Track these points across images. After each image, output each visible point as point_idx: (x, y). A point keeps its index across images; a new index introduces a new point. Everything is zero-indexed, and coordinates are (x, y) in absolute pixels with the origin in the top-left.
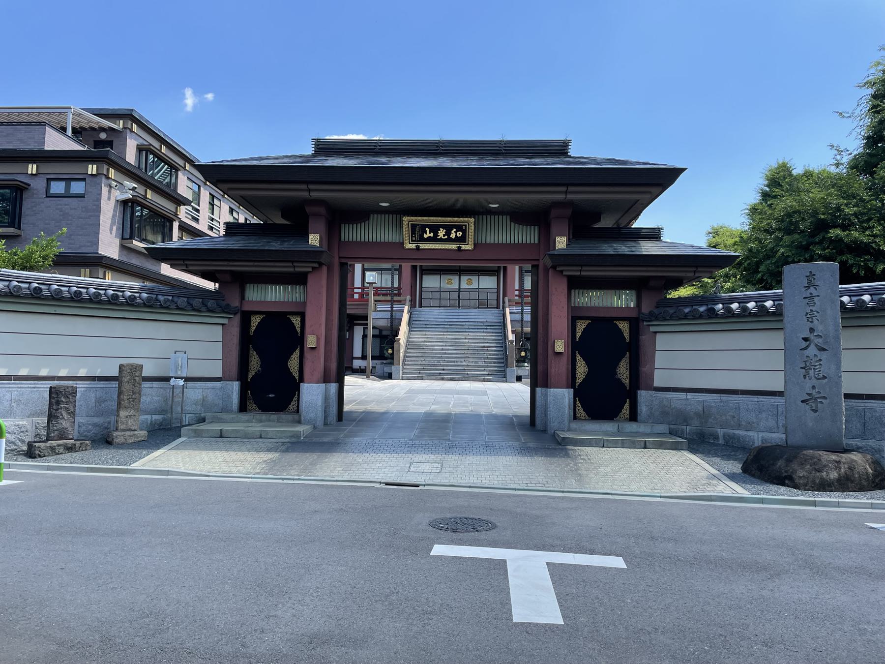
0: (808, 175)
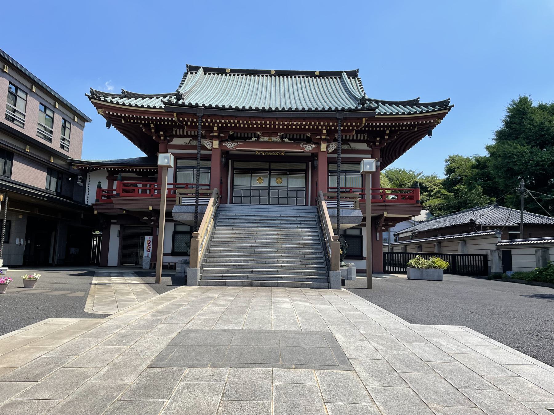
0: (542, 107)
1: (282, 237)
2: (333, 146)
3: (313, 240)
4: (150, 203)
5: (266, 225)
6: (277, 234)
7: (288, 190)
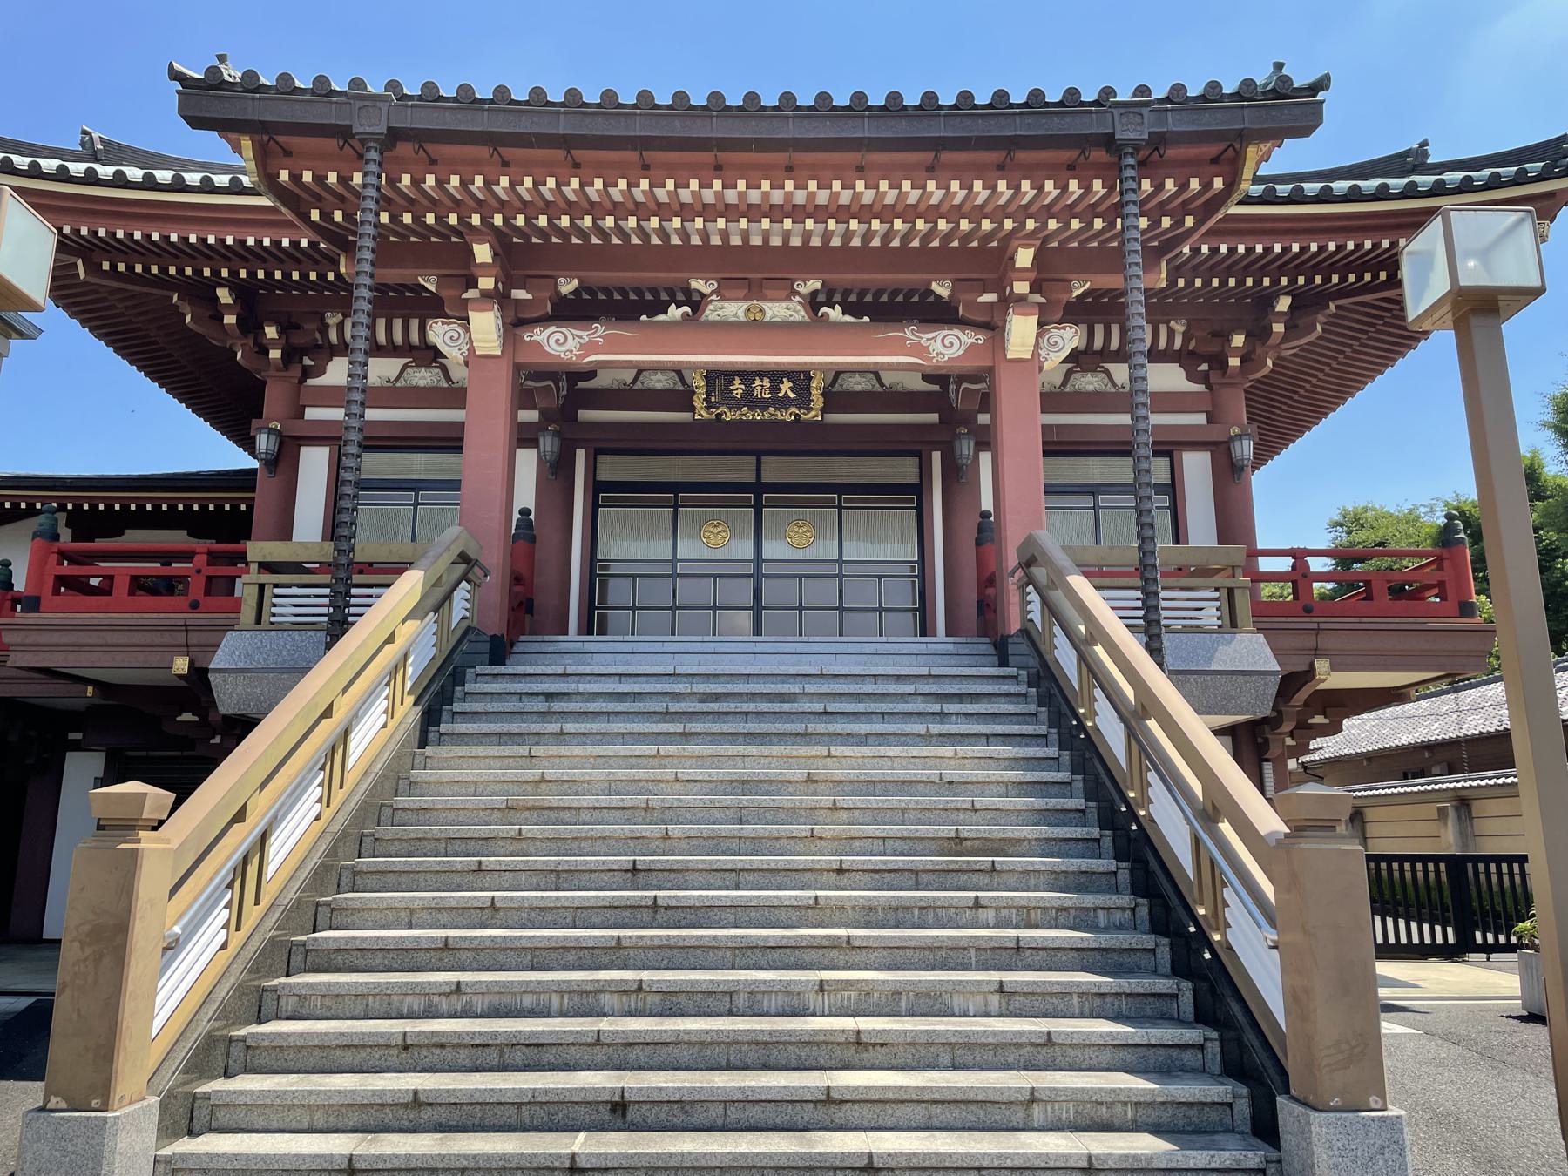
1: (844, 801)
2: (1069, 338)
3: (1045, 817)
4: (181, 638)
5: (741, 727)
6: (810, 780)
7: (840, 576)
